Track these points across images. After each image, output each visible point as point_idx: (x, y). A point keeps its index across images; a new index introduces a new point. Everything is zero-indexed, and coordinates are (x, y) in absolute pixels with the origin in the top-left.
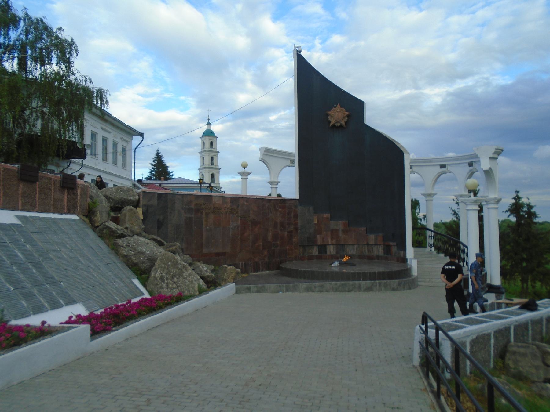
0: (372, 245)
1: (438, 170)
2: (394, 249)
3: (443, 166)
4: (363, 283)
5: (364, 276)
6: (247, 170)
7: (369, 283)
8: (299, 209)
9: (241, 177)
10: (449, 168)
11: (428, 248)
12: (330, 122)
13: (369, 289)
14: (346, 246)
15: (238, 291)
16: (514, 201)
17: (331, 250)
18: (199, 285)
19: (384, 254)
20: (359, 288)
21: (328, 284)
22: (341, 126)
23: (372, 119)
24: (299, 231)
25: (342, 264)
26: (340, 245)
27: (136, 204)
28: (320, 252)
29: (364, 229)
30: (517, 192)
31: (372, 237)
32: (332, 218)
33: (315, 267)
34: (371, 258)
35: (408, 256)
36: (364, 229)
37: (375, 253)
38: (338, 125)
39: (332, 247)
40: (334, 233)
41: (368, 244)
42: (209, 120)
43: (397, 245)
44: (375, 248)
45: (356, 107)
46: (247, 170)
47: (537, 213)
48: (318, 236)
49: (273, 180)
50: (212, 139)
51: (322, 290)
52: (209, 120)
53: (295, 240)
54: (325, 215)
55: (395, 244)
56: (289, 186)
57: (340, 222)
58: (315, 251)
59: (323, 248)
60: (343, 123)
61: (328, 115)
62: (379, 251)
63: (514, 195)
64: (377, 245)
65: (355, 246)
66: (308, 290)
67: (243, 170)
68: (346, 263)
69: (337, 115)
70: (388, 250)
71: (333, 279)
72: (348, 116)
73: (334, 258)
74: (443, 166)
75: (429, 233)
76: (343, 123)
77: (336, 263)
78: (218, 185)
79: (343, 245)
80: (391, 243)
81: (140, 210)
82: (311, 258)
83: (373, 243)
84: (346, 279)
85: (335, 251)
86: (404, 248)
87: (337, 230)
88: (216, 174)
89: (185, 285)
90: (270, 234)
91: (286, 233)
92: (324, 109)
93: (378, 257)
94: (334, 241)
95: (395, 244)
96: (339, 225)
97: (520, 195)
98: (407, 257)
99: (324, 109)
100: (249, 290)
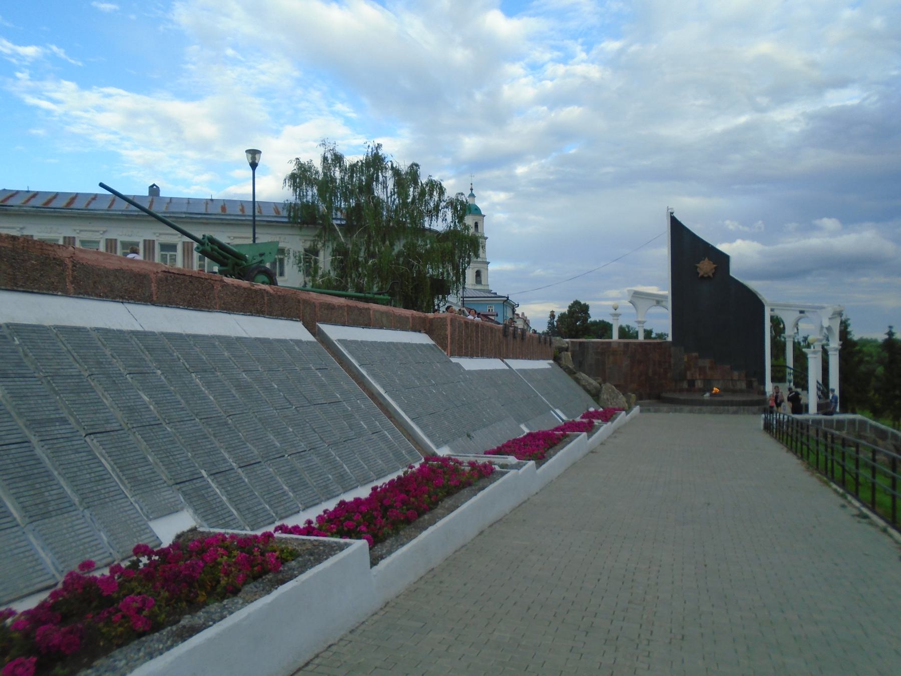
1: (798, 315)
2: (755, 384)
3: (802, 312)
4: (730, 408)
5: (732, 403)
6: (618, 311)
7: (735, 408)
8: (673, 349)
10: (807, 314)
11: (787, 384)
12: (698, 273)
13: (735, 413)
15: (641, 411)
16: (887, 337)
17: (699, 384)
20: (728, 412)
21: (705, 408)
23: (735, 270)
25: (712, 395)
27: (567, 350)
29: (728, 366)
30: (891, 327)
31: (736, 374)
33: (696, 397)
34: (734, 392)
35: (767, 390)
36: (728, 366)
40: (702, 370)
41: (732, 380)
42: (472, 190)
45: (723, 259)
46: (618, 311)
49: (640, 319)
50: (477, 218)
51: (700, 412)
52: (472, 190)
53: (669, 375)
54: (695, 354)
56: (661, 322)
58: (685, 385)
59: (692, 383)
60: (711, 275)
61: (697, 267)
62: (743, 385)
63: (887, 330)
66: (691, 412)
67: (613, 311)
68: (716, 394)
69: (706, 267)
70: (750, 385)
71: (707, 405)
72: (715, 268)
73: (704, 391)
74: (802, 312)
75: (788, 370)
76: (711, 275)
77: (707, 395)
78: (486, 288)
81: (569, 353)
82: (681, 391)
84: (719, 405)
86: (763, 382)
88: (482, 270)
90: (650, 371)
92: (690, 252)
96: (706, 363)
97: (894, 330)
99: (690, 252)
100: (649, 411)
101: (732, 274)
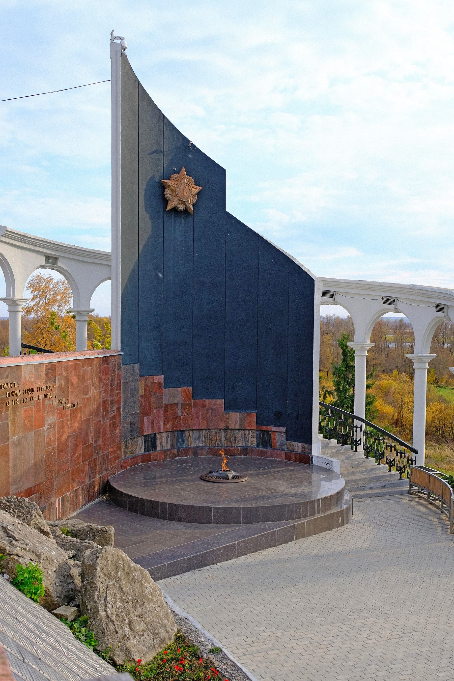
0: (233, 429)
9: (7, 307)
14: (187, 432)
17: (164, 442)
18: (76, 517)
19: (258, 445)
22: (186, 212)
23: (239, 203)
24: (122, 413)
26: (177, 431)
28: (147, 449)
31: (235, 418)
32: (167, 384)
37: (241, 444)
38: (182, 208)
39: (164, 435)
41: (226, 429)
43: (286, 432)
44: (239, 435)
45: (212, 177)
47: (435, 308)
48: (145, 418)
55: (284, 429)
57: (180, 389)
59: (151, 442)
64: (244, 430)
65: (204, 432)
69: (184, 191)
70: (265, 440)
79: (182, 432)
80: (274, 429)
83: (238, 427)
85: (170, 442)
87: (175, 405)
89: (14, 574)
91: (108, 422)
93: (246, 451)
94: (169, 425)
95: (284, 429)
96: (177, 395)
98: (313, 453)
101: (228, 209)
